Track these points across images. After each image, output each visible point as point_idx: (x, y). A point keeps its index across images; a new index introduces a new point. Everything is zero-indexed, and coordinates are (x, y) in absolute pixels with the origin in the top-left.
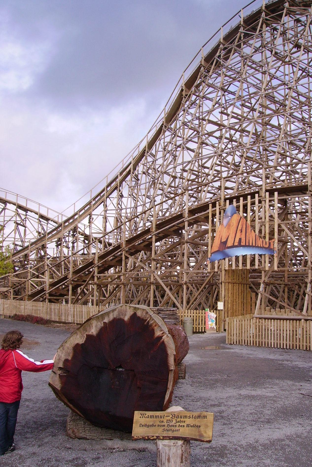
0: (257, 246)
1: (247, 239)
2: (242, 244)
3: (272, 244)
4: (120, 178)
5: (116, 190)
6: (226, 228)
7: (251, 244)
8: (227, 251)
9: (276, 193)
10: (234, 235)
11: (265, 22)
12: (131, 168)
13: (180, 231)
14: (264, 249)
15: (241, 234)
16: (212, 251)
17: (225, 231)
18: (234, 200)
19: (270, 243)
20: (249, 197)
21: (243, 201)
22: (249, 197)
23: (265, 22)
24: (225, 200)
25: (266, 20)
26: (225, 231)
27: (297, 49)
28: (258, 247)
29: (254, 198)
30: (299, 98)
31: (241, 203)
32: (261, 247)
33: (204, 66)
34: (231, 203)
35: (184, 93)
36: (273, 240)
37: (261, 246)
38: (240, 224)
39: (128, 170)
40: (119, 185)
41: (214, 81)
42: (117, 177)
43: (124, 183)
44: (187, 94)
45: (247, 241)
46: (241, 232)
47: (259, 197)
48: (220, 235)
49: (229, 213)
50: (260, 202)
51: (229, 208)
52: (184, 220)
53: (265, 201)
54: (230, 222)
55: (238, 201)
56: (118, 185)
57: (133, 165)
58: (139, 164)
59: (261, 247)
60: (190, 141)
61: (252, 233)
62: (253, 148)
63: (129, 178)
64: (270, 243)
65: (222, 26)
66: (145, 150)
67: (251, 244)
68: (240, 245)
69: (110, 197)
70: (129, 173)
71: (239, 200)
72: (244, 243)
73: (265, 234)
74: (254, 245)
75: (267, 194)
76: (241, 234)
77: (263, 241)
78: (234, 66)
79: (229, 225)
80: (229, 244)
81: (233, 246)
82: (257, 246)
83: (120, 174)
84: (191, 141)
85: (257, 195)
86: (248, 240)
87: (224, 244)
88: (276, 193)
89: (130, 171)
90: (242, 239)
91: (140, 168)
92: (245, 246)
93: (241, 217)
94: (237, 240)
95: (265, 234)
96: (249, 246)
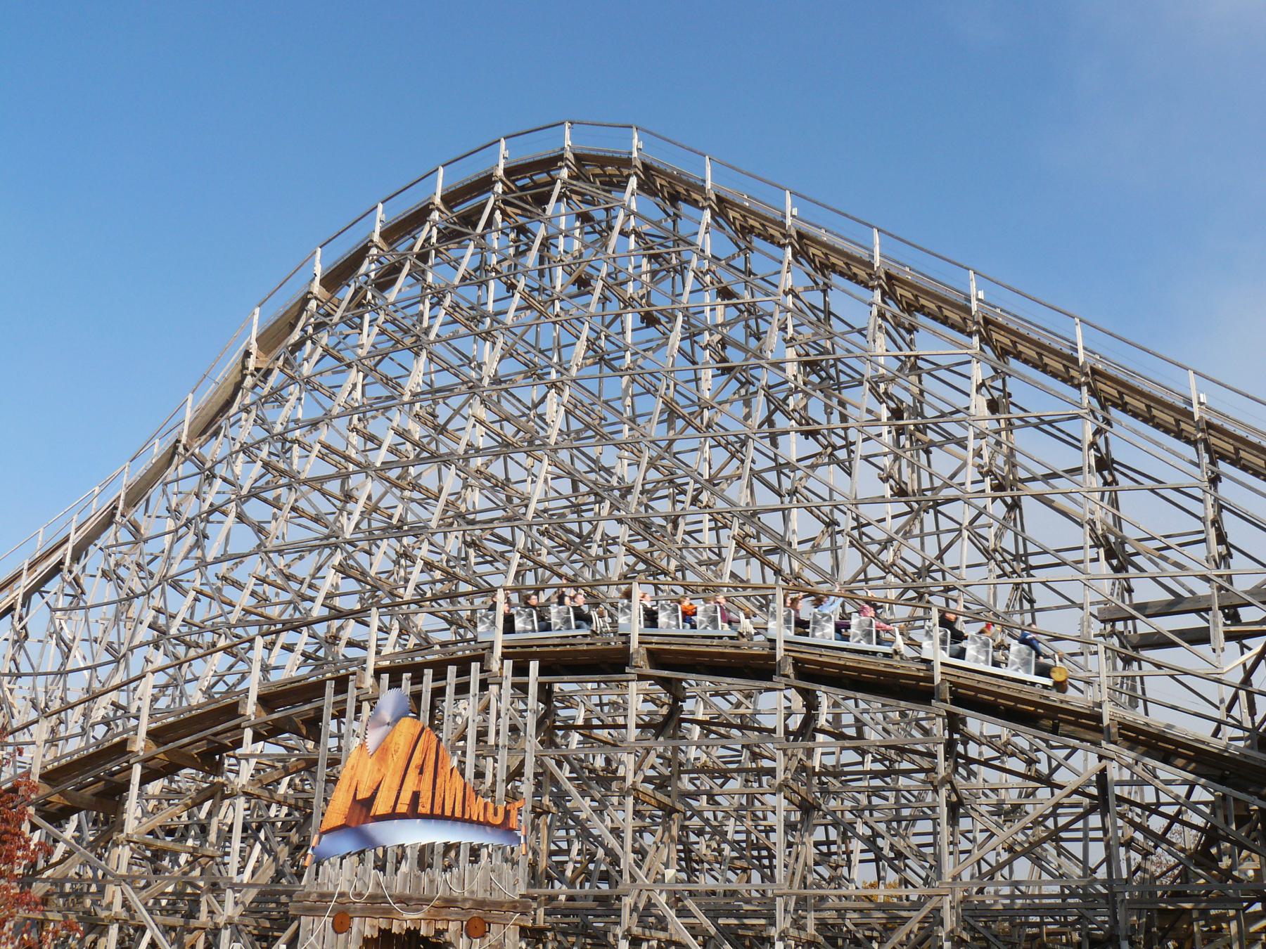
0: (467, 817)
1: (437, 794)
2: (421, 810)
3: (514, 813)
4: (25, 582)
5: (9, 616)
6: (374, 757)
7: (448, 813)
8: (372, 827)
9: (534, 666)
10: (397, 781)
11: (500, 208)
12: (65, 555)
13: (217, 757)
14: (488, 828)
15: (420, 781)
16: (325, 826)
17: (369, 765)
18: (407, 676)
19: (507, 813)
20: (429, 673)
21: (434, 680)
22: (429, 673)
23: (500, 208)
24: (378, 673)
25: (506, 202)
26: (369, 765)
27: (579, 289)
28: (470, 821)
29: (468, 673)
30: (502, 428)
31: (428, 684)
32: (478, 823)
33: (316, 298)
34: (395, 683)
35: (251, 363)
36: (517, 804)
37: (481, 819)
38: (418, 747)
39: (54, 559)
40: (20, 601)
41: (339, 343)
42: (17, 577)
43: (36, 597)
44: (259, 366)
45: (438, 800)
46: (421, 773)
47: (482, 671)
48: (352, 779)
49: (387, 714)
50: (484, 685)
51: (389, 699)
52: (243, 725)
53: (500, 685)
54: (388, 740)
55: (417, 679)
56: (17, 600)
57: (74, 548)
58: (91, 548)
59: (478, 823)
60: (253, 496)
61: (454, 779)
62: (496, 531)
63: (54, 585)
64: (507, 813)
65: (384, 198)
66: (116, 508)
67: (437, 811)
68: (413, 813)
69: (1245, 642)
70: (57, 569)
71: (422, 677)
72: (429, 807)
73: (494, 783)
74: (458, 814)
75: (509, 664)
76: (420, 781)
77: (486, 805)
78: (403, 308)
79: (383, 750)
80: (381, 807)
81: (392, 816)
82: (467, 817)
83: (29, 569)
84: (256, 496)
85: (475, 666)
86: (441, 799)
87: (363, 806)
88: (534, 666)
89: (61, 562)
90: (422, 795)
91: (95, 559)
92: (430, 817)
93: (423, 729)
94: (406, 797)
95: (494, 783)
96: (442, 817)
